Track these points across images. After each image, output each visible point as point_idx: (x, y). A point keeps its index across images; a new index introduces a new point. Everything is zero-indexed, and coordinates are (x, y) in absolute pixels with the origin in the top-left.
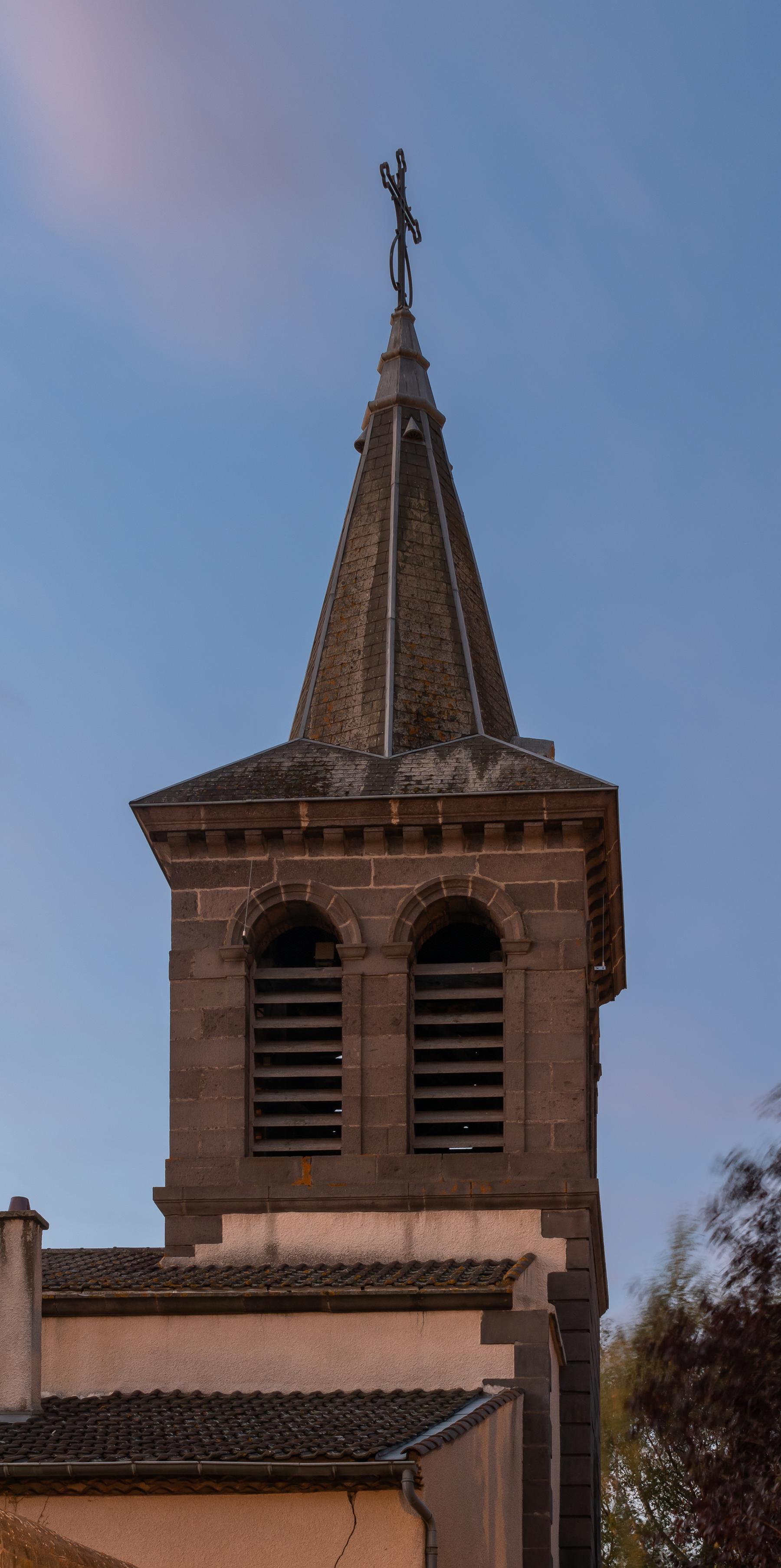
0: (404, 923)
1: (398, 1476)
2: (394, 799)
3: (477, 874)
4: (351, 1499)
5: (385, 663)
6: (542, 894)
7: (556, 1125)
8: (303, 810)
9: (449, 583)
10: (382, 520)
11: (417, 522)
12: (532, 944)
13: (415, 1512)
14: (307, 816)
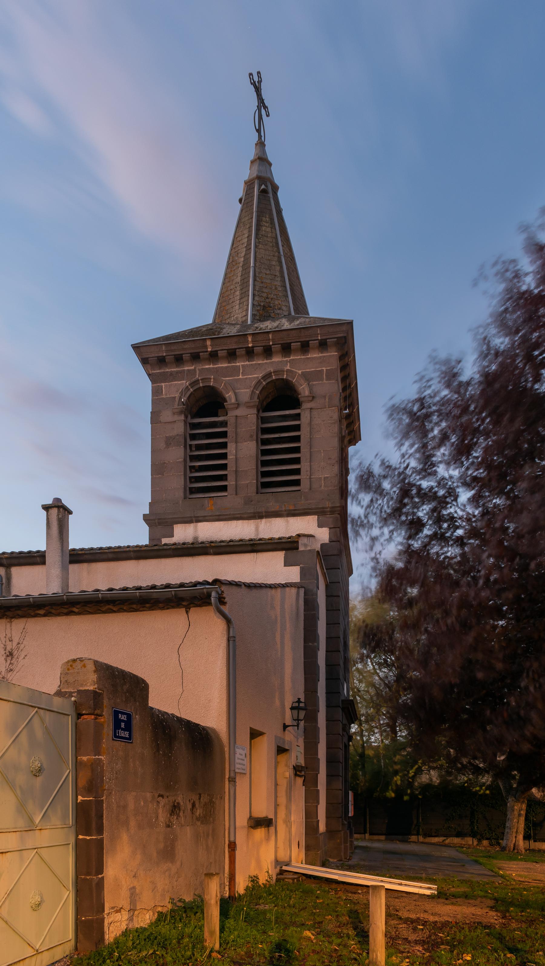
0: (255, 392)
1: (209, 595)
2: (249, 334)
3: (288, 368)
4: (187, 612)
5: (249, 286)
6: (317, 375)
7: (324, 478)
8: (209, 343)
9: (279, 252)
10: (249, 228)
11: (265, 227)
12: (313, 397)
13: (222, 617)
14: (210, 345)
